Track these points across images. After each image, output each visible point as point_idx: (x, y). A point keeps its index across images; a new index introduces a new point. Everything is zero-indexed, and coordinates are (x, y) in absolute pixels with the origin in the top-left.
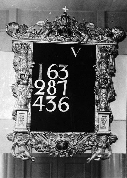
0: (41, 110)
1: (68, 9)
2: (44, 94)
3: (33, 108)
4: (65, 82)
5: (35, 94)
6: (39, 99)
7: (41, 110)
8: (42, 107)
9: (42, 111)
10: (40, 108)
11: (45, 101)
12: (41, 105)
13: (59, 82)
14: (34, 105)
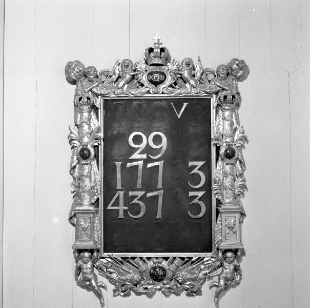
0: (121, 215)
1: (157, 34)
2: (130, 192)
3: (106, 212)
4: (160, 164)
5: (204, 192)
6: (118, 197)
7: (121, 215)
8: (123, 211)
9: (130, 195)
10: (139, 169)
11: (128, 200)
12: (122, 208)
13: (150, 165)
14: (109, 207)
